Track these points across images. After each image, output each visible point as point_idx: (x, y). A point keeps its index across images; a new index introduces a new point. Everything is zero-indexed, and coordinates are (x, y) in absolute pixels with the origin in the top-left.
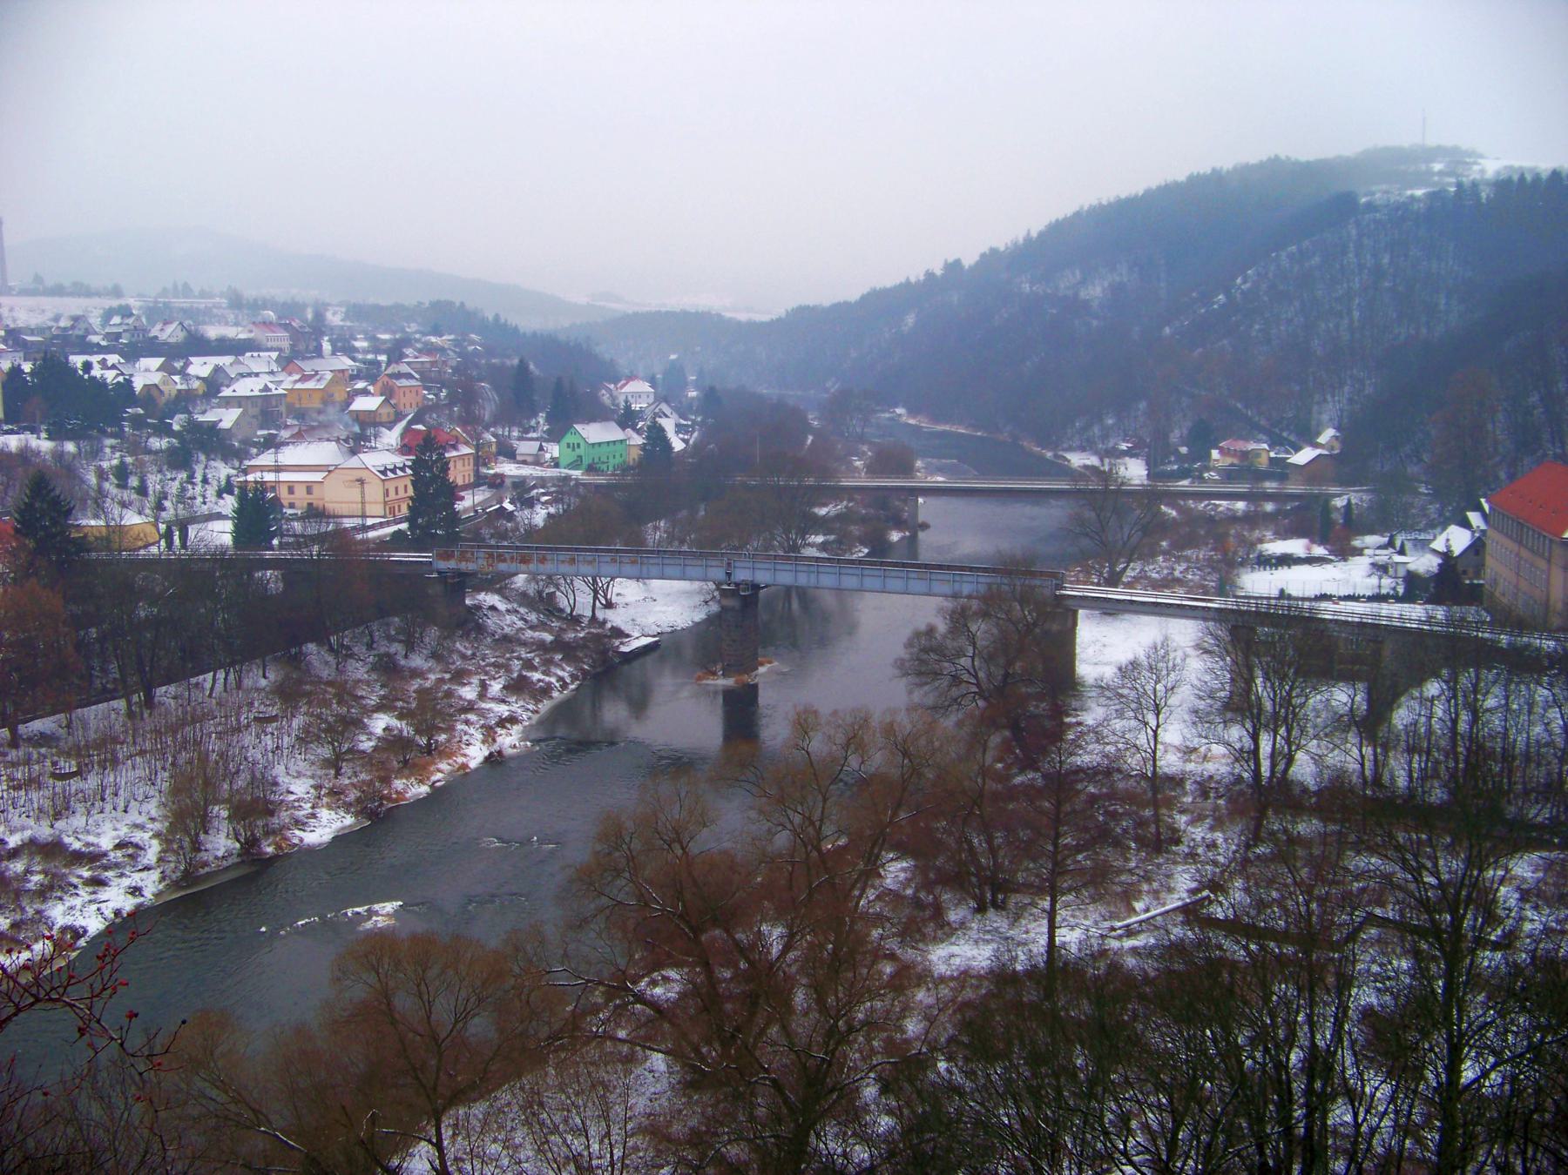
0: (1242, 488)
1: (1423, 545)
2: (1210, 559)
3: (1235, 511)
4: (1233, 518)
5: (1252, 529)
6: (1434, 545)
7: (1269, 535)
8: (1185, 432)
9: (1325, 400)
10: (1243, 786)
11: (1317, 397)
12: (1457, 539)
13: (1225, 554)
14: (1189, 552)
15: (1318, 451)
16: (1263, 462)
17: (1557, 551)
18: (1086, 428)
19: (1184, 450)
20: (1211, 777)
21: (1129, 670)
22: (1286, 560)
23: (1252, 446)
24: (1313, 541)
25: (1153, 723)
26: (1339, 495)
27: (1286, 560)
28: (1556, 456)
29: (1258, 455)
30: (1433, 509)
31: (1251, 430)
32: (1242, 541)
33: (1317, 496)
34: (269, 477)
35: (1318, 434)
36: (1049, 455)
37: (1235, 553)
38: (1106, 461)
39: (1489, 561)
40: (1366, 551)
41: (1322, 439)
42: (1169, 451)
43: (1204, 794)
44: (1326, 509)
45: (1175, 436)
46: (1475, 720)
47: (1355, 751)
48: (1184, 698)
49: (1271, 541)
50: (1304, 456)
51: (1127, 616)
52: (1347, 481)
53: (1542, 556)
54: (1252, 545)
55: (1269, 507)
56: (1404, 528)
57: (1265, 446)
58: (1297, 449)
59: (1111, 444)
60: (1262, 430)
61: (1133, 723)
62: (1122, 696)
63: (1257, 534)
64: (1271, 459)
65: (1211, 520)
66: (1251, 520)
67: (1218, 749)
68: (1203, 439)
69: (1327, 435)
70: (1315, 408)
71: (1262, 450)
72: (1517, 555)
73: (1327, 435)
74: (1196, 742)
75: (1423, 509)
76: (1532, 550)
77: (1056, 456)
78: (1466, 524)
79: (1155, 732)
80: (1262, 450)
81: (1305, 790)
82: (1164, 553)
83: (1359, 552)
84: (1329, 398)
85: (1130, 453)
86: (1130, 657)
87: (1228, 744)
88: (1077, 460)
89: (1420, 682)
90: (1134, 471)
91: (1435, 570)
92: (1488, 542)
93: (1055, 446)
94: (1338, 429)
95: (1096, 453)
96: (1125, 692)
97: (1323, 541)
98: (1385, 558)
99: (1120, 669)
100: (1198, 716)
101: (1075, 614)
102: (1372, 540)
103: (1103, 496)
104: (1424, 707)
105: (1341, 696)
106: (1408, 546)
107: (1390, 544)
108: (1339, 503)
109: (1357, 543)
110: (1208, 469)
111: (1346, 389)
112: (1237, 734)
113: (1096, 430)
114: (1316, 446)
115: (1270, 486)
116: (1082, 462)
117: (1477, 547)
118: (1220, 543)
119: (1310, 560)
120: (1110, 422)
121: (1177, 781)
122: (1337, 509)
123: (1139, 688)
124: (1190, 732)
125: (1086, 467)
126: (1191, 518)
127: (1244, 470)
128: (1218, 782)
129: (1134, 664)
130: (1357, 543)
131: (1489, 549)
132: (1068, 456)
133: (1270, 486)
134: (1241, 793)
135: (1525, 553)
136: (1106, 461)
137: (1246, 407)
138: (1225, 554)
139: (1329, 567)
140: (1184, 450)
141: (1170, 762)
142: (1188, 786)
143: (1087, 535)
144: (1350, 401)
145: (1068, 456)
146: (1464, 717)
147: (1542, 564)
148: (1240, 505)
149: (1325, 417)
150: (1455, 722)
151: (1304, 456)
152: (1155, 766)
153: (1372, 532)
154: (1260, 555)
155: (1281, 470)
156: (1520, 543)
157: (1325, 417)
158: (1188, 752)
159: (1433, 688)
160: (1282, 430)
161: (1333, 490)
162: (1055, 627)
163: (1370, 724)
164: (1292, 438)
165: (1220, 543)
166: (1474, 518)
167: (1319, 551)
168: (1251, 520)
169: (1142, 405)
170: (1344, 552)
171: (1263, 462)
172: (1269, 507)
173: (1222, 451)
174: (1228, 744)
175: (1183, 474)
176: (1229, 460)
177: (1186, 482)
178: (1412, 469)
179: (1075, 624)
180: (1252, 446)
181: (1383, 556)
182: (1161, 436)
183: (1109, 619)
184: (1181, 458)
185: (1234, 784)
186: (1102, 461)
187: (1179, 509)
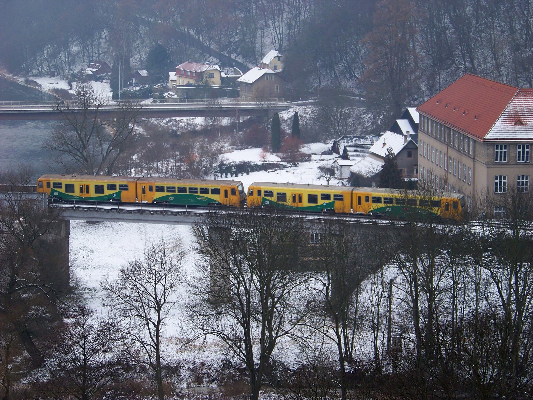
0: (201, 105)
1: (363, 150)
2: (178, 169)
3: (195, 126)
4: (194, 133)
5: (211, 141)
6: (372, 149)
7: (227, 146)
8: (144, 56)
9: (266, 26)
10: (232, 370)
11: (261, 23)
12: (393, 143)
13: (191, 164)
14: (156, 164)
15: (265, 71)
16: (216, 82)
17: (481, 151)
18: (54, 55)
19: (144, 73)
20: (203, 364)
21: (130, 273)
22: (245, 168)
23: (205, 67)
24: (266, 150)
25: (154, 317)
26: (286, 109)
27: (245, 168)
28: (466, 69)
29: (211, 76)
30: (367, 118)
31: (204, 53)
32: (204, 152)
33: (265, 111)
34: (258, 103)
35: (262, 56)
36: (21, 80)
37: (200, 163)
38: (74, 85)
39: (421, 161)
40: (313, 157)
41: (266, 60)
42: (130, 75)
43: (198, 379)
44: (277, 121)
45: (135, 61)
46: (431, 299)
47: (332, 333)
48: (180, 294)
49: (228, 151)
50: (252, 75)
51: (109, 224)
52: (293, 96)
53: (468, 155)
54: (214, 155)
55: (225, 121)
56: (346, 135)
57: (217, 67)
58: (246, 70)
59: (77, 70)
60: (212, 53)
61: (138, 320)
62: (125, 296)
63: (215, 146)
64: (222, 79)
65: (174, 134)
66: (210, 133)
67: (211, 338)
68: (161, 62)
69: (270, 56)
70: (259, 33)
71: (214, 70)
72: (446, 155)
73: (270, 56)
74: (193, 334)
75: (358, 118)
76: (459, 151)
77: (27, 81)
78: (397, 130)
79: (157, 327)
80: (214, 70)
81: (286, 370)
82: (136, 166)
83: (307, 158)
84: (270, 23)
85: (95, 77)
86: (132, 260)
87: (221, 333)
88: (47, 84)
89: (376, 268)
90: (101, 92)
91: (380, 168)
92: (420, 145)
93: (26, 73)
94: (280, 50)
95: (64, 77)
96: (129, 292)
97: (275, 150)
98: (331, 162)
99: (123, 272)
100: (194, 311)
101: (67, 223)
102: (317, 147)
103: (80, 119)
104: (388, 289)
105: (318, 285)
106: (350, 151)
107: (335, 149)
108: (286, 115)
109: (305, 149)
110: (168, 90)
111: (285, 15)
112: (229, 323)
113: (63, 57)
114: (264, 66)
115: (225, 102)
116: (51, 87)
117: (410, 149)
118: (186, 155)
119: (266, 167)
120: (76, 49)
121: (174, 370)
122: (285, 121)
123: (140, 287)
124: (188, 326)
125: (56, 91)
126: (158, 135)
127: (200, 89)
128: (208, 368)
129: (135, 267)
130: (305, 149)
131: (420, 151)
132: (39, 81)
133: (225, 102)
134: (231, 376)
135: (453, 153)
136: (74, 85)
137: (199, 33)
138: (191, 164)
139: (282, 172)
140: (144, 73)
141: (170, 353)
142: (184, 373)
143: (70, 152)
144: (289, 26)
145: (39, 81)
146: (423, 297)
147: (468, 162)
148: (199, 121)
149: (267, 40)
150: (415, 301)
151: (252, 75)
152: (158, 357)
153: (316, 140)
154: (222, 165)
155: (232, 88)
156: (448, 145)
157: (267, 40)
158: (187, 343)
159: (391, 271)
160: (230, 53)
161: (281, 104)
162: (50, 237)
163: (338, 308)
164: (240, 59)
165: (186, 155)
166: (403, 124)
167: (272, 158)
168: (210, 133)
169: (105, 34)
170: (295, 159)
171: (216, 82)
172: (225, 121)
173: (178, 72)
174: (221, 333)
175: (146, 94)
176: (185, 81)
177: (149, 101)
178: (349, 84)
179: (68, 234)
180: (205, 67)
181: (329, 161)
182: (123, 60)
183: (93, 227)
184: (142, 80)
185: (223, 369)
186: (70, 85)
187: (146, 127)
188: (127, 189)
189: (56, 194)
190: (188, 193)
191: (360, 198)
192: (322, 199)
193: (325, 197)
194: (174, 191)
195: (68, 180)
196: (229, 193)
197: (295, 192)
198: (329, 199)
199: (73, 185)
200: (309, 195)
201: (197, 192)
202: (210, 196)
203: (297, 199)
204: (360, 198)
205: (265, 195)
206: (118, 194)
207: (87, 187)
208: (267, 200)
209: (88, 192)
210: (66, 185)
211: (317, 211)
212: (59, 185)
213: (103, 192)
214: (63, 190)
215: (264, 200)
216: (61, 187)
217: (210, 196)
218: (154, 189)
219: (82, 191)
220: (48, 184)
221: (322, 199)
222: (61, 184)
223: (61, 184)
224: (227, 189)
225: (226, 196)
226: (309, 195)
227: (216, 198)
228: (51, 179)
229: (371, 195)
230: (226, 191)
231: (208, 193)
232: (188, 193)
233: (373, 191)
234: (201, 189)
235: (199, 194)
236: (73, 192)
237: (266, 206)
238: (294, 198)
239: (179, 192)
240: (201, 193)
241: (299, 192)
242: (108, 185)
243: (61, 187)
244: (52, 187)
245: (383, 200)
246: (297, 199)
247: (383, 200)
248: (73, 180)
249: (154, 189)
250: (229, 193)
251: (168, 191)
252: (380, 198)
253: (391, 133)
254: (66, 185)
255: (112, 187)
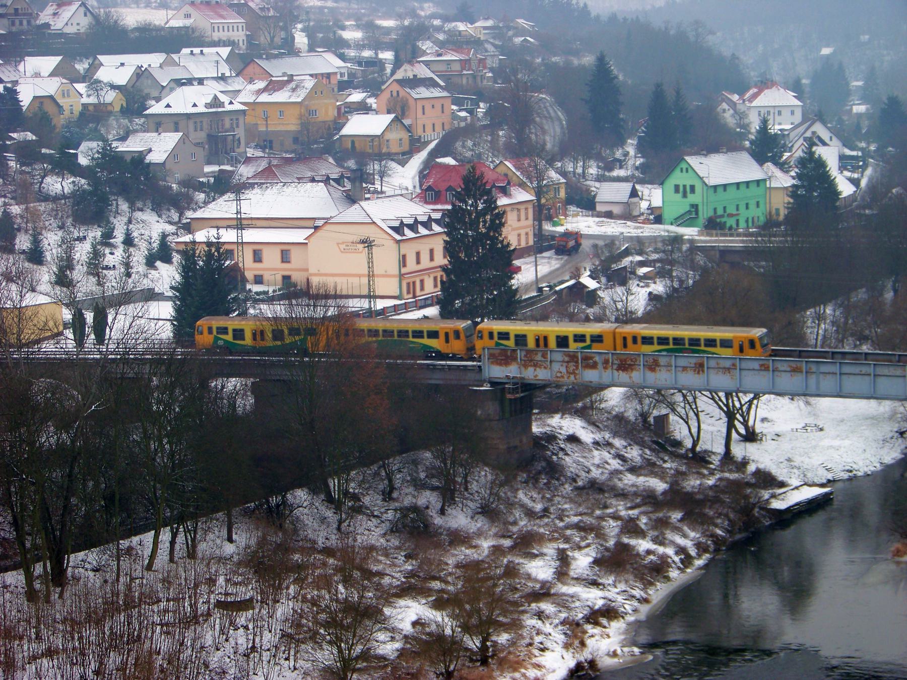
188: (601, 341)
189: (220, 343)
190: (396, 338)
191: (625, 339)
192: (575, 341)
193: (294, 331)
194: (668, 344)
195: (236, 323)
196: (451, 336)
197: (539, 333)
198: (584, 341)
199: (242, 330)
200: (558, 337)
201: (699, 345)
202: (426, 341)
203: (542, 342)
204: (625, 339)
205: (499, 338)
206: (304, 341)
207: (546, 338)
208: (221, 339)
209: (263, 339)
210: (234, 330)
211: (285, 351)
212: (224, 330)
213: (567, 346)
214: (229, 337)
215: (497, 344)
216: (227, 333)
217: (426, 341)
218: (639, 340)
219: (254, 339)
220: (210, 330)
221: (575, 341)
222: (226, 328)
223: (226, 328)
224: (448, 331)
225: (447, 341)
226: (558, 337)
227: (433, 343)
228: (213, 322)
229: (640, 334)
230: (447, 334)
231: (422, 337)
232: (687, 346)
233: (644, 328)
234: (414, 332)
235: (411, 339)
236: (244, 339)
237: (220, 347)
238: (537, 341)
239: (674, 344)
240: (414, 337)
241: (545, 334)
242: (575, 336)
243: (227, 333)
244: (215, 333)
245: (655, 341)
246: (542, 342)
247: (655, 341)
248: (243, 323)
249: (639, 340)
250: (746, 346)
251: (659, 344)
252: (652, 338)
253: (750, 157)
254: (234, 330)
255: (580, 338)
